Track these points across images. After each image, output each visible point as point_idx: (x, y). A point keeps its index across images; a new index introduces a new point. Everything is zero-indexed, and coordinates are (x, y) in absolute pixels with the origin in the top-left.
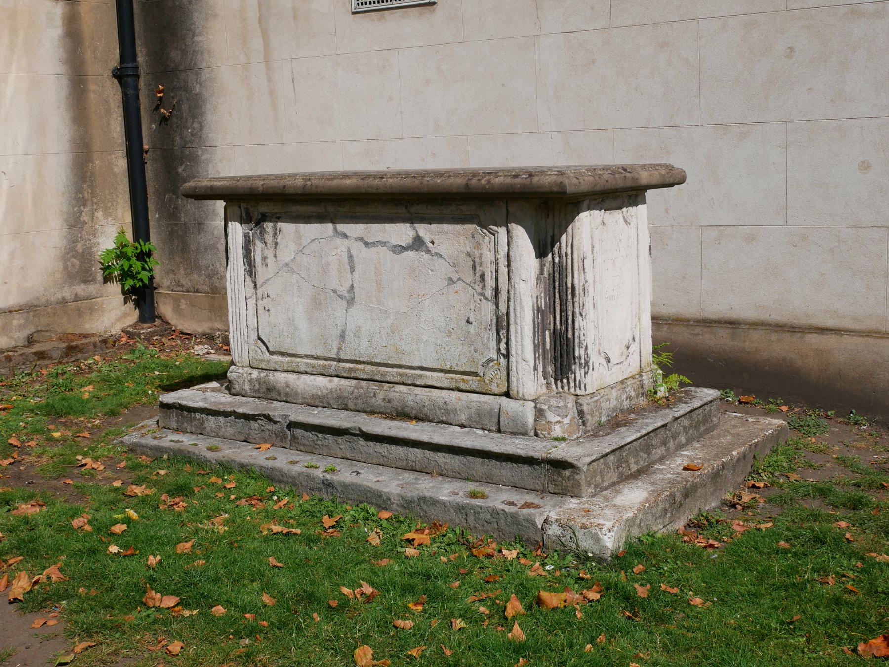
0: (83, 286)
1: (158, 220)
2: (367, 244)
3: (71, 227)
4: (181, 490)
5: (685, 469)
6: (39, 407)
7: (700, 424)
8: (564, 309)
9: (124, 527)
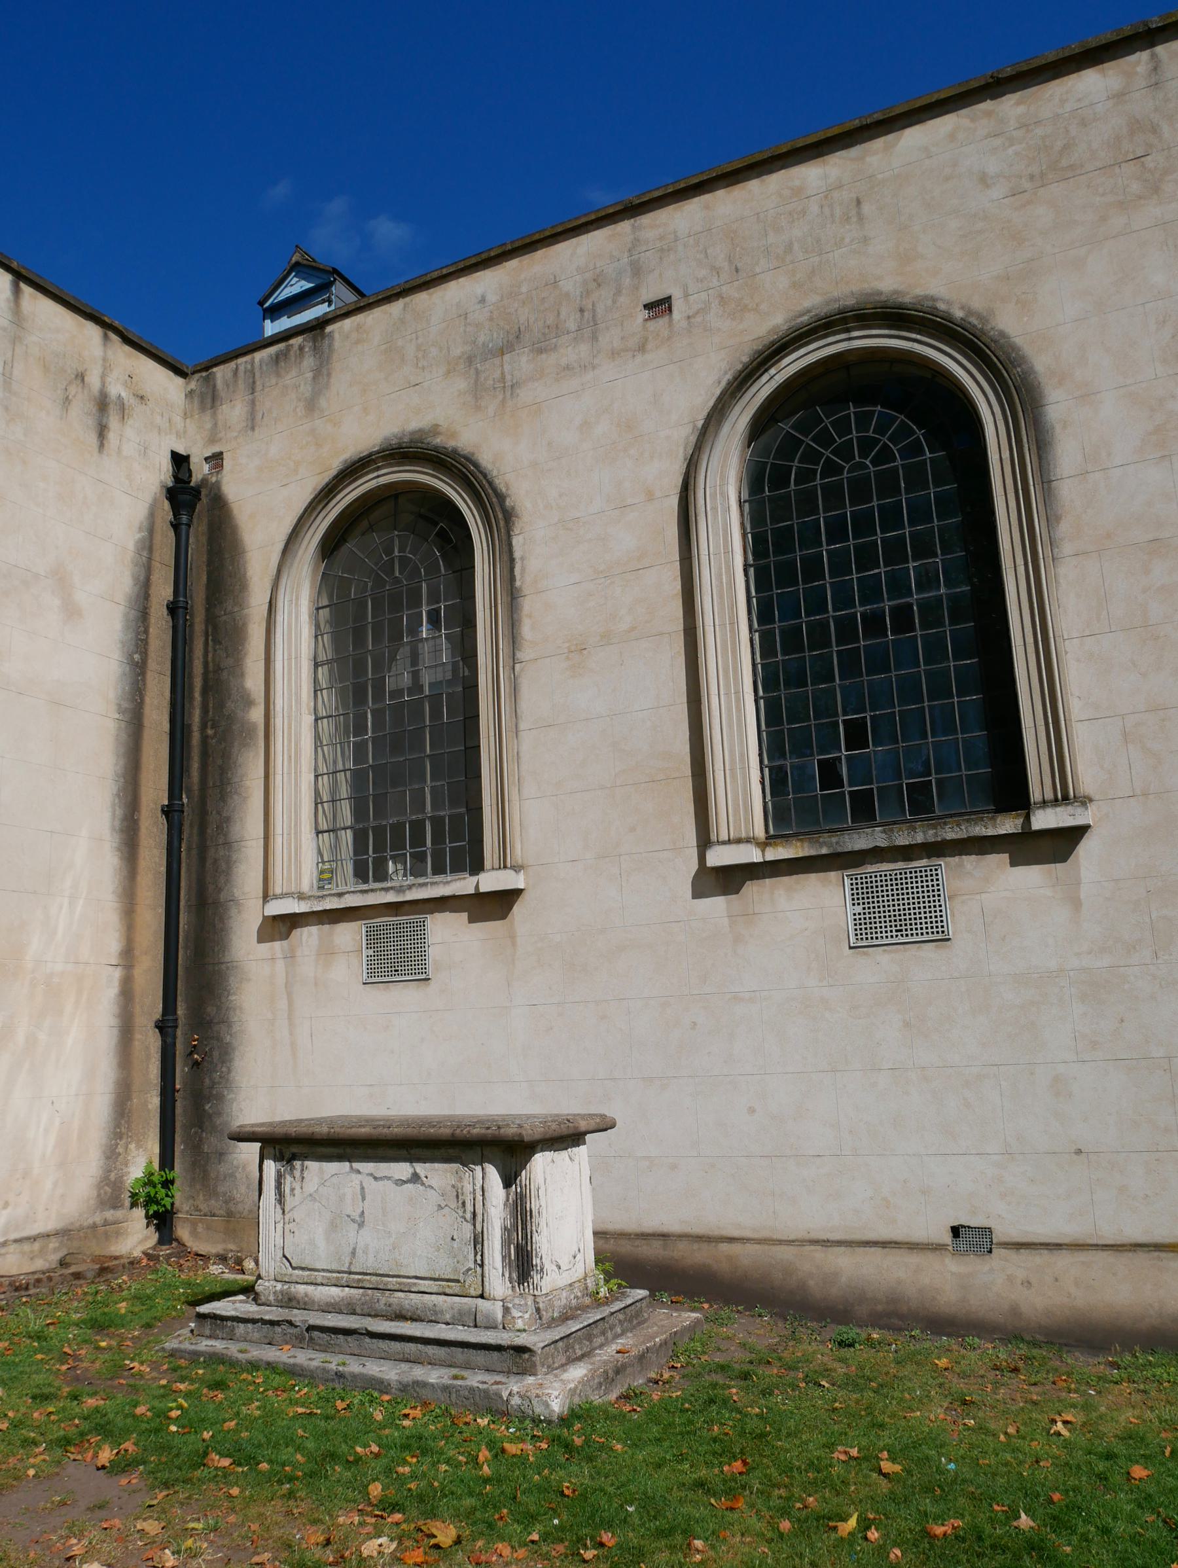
0: (112, 1211)
1: (183, 1151)
2: (375, 1178)
3: (108, 1158)
4: (219, 1385)
5: (618, 1352)
6: (84, 1322)
7: (633, 1318)
8: (524, 1228)
9: (179, 1412)
